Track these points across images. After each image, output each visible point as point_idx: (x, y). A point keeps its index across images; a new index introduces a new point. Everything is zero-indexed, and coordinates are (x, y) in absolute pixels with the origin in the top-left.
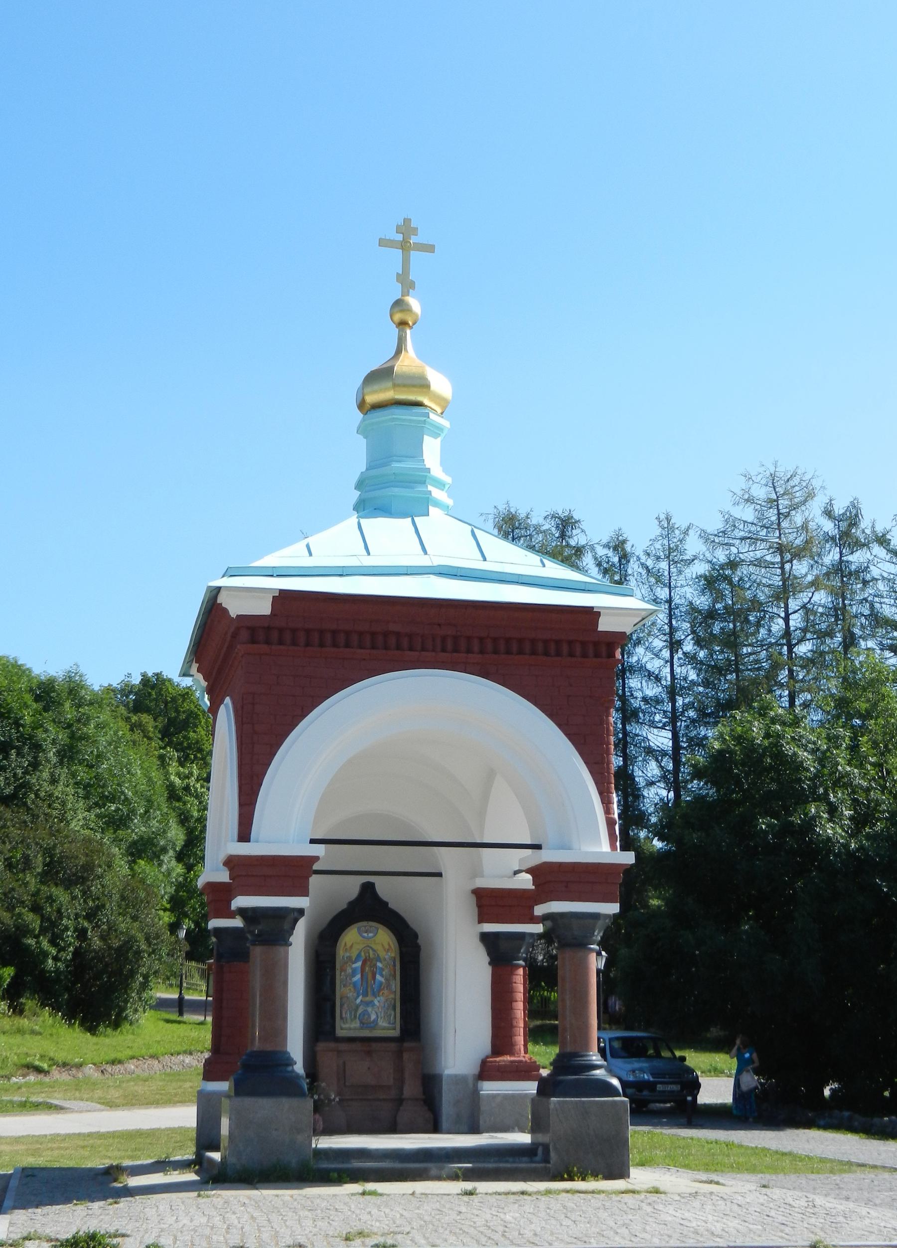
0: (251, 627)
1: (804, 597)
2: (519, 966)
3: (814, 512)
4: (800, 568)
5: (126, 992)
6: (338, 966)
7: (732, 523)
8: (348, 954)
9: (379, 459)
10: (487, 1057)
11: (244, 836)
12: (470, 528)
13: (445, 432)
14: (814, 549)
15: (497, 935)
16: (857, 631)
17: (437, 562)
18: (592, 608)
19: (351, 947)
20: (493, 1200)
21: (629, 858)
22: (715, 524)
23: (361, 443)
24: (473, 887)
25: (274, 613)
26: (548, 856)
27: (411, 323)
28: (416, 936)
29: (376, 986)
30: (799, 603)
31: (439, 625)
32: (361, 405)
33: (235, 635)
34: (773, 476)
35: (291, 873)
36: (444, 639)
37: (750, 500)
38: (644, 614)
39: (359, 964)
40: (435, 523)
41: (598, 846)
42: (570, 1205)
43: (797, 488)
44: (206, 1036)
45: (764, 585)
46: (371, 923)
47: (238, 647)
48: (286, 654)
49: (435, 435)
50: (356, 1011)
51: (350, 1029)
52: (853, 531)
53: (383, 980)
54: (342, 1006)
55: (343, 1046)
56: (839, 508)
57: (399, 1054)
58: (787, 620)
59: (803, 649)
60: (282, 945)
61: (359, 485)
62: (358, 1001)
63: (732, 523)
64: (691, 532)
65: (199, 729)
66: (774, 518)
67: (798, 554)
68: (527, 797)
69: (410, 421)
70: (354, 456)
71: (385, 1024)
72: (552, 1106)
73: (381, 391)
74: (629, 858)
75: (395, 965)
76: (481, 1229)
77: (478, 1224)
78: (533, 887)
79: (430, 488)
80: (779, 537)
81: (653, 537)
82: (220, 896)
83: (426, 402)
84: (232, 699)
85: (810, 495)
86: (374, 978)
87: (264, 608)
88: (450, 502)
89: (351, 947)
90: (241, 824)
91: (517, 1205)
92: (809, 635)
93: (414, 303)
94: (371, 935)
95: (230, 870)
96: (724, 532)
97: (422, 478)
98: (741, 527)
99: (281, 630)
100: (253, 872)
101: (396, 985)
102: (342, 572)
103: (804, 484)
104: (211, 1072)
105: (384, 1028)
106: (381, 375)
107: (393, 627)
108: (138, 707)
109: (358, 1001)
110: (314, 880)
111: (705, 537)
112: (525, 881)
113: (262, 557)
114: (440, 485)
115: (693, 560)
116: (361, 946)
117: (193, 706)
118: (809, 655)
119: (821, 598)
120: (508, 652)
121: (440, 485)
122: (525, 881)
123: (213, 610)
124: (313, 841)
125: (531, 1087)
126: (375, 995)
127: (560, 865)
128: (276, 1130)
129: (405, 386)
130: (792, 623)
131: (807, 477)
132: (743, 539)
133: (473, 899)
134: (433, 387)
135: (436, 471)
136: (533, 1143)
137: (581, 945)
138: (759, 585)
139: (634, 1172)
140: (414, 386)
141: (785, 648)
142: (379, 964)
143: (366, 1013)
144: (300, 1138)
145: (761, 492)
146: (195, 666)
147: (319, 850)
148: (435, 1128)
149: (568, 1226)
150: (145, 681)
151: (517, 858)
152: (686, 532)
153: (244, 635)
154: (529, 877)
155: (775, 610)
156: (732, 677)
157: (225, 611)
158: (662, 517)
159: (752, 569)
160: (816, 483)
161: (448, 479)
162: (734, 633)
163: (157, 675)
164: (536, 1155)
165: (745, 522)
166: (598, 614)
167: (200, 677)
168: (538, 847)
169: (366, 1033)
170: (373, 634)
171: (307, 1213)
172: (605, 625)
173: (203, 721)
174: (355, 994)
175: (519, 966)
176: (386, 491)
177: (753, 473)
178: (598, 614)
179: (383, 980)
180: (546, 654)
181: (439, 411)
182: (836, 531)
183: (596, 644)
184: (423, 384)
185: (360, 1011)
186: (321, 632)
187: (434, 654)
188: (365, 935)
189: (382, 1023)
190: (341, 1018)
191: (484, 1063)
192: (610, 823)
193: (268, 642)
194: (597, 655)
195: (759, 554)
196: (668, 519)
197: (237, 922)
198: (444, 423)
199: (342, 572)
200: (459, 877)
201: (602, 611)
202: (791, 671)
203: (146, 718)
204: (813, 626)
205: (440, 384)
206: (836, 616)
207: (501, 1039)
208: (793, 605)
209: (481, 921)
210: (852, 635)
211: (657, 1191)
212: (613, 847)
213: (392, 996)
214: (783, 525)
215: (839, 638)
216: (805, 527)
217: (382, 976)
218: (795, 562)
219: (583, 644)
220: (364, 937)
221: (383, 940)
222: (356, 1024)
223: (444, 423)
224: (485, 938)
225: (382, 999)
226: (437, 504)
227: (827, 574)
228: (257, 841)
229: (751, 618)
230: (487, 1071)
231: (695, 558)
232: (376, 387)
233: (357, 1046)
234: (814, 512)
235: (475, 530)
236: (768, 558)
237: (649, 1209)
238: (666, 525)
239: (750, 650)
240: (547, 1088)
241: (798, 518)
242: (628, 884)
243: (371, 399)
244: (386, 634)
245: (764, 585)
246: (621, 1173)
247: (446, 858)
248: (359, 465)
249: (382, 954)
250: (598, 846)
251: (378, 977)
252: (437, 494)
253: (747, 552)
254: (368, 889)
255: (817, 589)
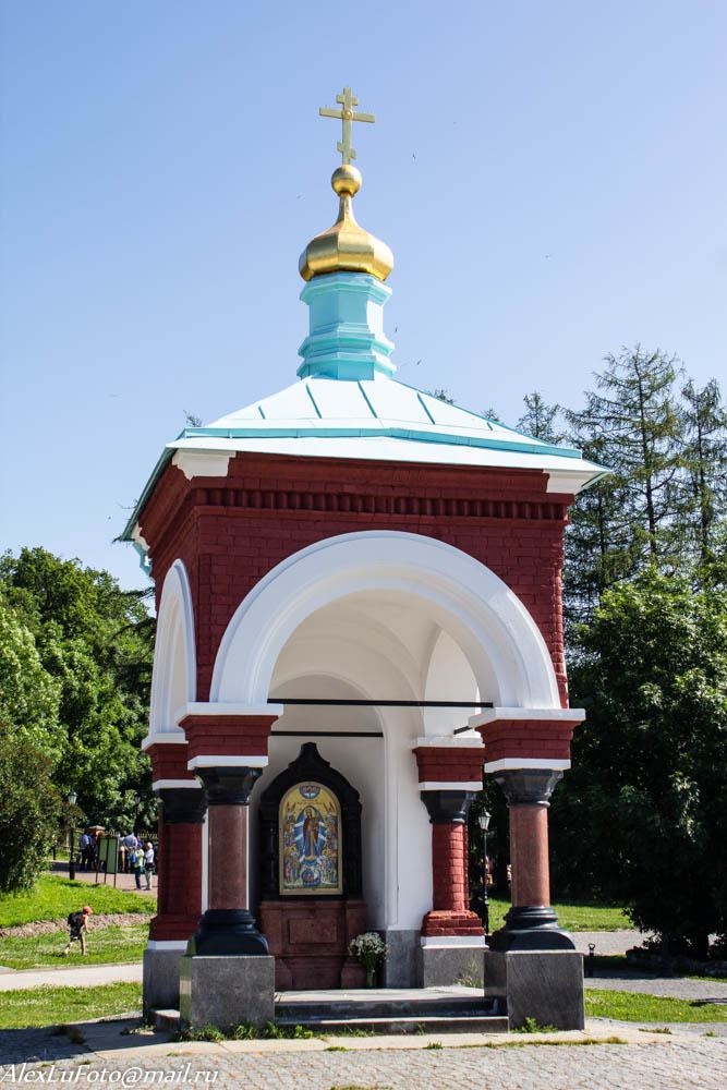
0: (207, 489)
1: (665, 474)
2: (459, 824)
3: (674, 395)
4: (661, 446)
5: (21, 858)
6: (281, 826)
7: (596, 403)
8: (290, 814)
9: (324, 324)
10: (429, 913)
11: (203, 695)
12: (415, 393)
13: (388, 298)
14: (674, 428)
15: (438, 793)
16: (716, 507)
17: (387, 425)
18: (542, 470)
19: (294, 806)
20: (459, 1054)
21: (579, 715)
22: (581, 406)
23: (304, 310)
24: (414, 747)
25: (230, 475)
26: (502, 713)
27: (352, 191)
28: (357, 795)
29: (318, 845)
30: (661, 479)
31: (393, 487)
32: (304, 271)
33: (188, 498)
34: (635, 359)
35: (249, 732)
36: (397, 500)
37: (614, 382)
38: (591, 475)
39: (302, 824)
40: (380, 386)
41: (546, 702)
42: (540, 1057)
43: (658, 370)
44: (152, 895)
45: (629, 463)
46: (313, 783)
47: (195, 508)
48: (229, 521)
49: (379, 301)
50: (299, 869)
51: (293, 888)
52: (711, 411)
53: (325, 839)
54: (285, 865)
55: (288, 905)
56: (698, 389)
57: (342, 911)
58: (649, 495)
59: (665, 523)
60: (241, 804)
61: (303, 351)
62: (301, 860)
63: (596, 403)
64: (558, 413)
65: (79, 603)
66: (636, 399)
67: (658, 434)
68: (485, 658)
69: (324, 289)
70: (298, 325)
71: (327, 883)
72: (508, 960)
73: (326, 257)
74: (579, 715)
75: (336, 825)
76: (463, 1082)
77: (457, 1078)
78: (483, 746)
79: (374, 353)
80: (642, 417)
81: (522, 417)
82: (169, 759)
83: (368, 267)
84: (184, 560)
85: (669, 378)
86: (316, 837)
87: (220, 470)
88: (393, 368)
89: (294, 806)
90: (199, 684)
91: (487, 1058)
92: (670, 510)
93: (353, 171)
94: (312, 794)
95: (186, 731)
96: (589, 413)
97: (365, 344)
98: (605, 407)
99: (237, 492)
100: (203, 732)
101: (338, 844)
102: (297, 434)
103: (665, 366)
104: (157, 931)
105: (327, 887)
106: (327, 242)
107: (349, 489)
108: (19, 581)
109: (301, 860)
110: (271, 740)
111: (572, 417)
112: (473, 739)
113: (215, 420)
114: (383, 350)
115: (560, 439)
116: (303, 807)
117: (71, 581)
118: (671, 529)
119: (682, 474)
120: (460, 513)
121: (383, 350)
122: (473, 739)
123: (167, 471)
124: (270, 701)
125: (479, 943)
126: (317, 854)
127: (513, 722)
128: (238, 988)
129: (349, 253)
130: (654, 499)
131: (667, 360)
132: (607, 418)
133: (414, 756)
134: (377, 255)
135: (380, 338)
136: (486, 997)
137: (532, 801)
138: (623, 462)
139: (588, 1023)
140: (358, 253)
141: (648, 522)
142: (321, 824)
143: (308, 872)
144: (262, 995)
145: (623, 374)
146: (138, 530)
147: (278, 710)
148: (379, 983)
149: (547, 1078)
150: (25, 557)
151: (462, 716)
152: (553, 413)
153: (201, 496)
154: (478, 735)
155: (638, 486)
156: (598, 550)
157: (181, 472)
158: (530, 398)
159: (616, 447)
160: (676, 367)
161: (391, 346)
162: (600, 509)
163: (38, 550)
164: (492, 1008)
165: (609, 402)
166: (548, 476)
167: (142, 541)
168: (490, 705)
169: (309, 892)
170: (328, 496)
171: (283, 1070)
172: (553, 487)
173: (82, 595)
174: (298, 854)
175: (459, 824)
176: (323, 356)
177: (617, 357)
178: (548, 476)
179: (325, 839)
180: (497, 515)
181: (382, 278)
182: (695, 411)
183: (545, 506)
184: (368, 253)
185: (303, 870)
186: (277, 493)
187: (387, 515)
188: (307, 794)
189: (325, 881)
190: (285, 876)
191: (426, 918)
192: (560, 680)
193: (224, 503)
194: (546, 517)
195: (622, 433)
196: (537, 399)
197: (197, 783)
198: (388, 290)
199: (297, 434)
200: (398, 739)
201: (551, 473)
202: (653, 544)
203: (24, 591)
204: (674, 501)
205: (384, 253)
206: (696, 492)
207: (442, 898)
208: (654, 481)
209: (421, 780)
210: (710, 509)
211: (617, 1041)
212: (564, 705)
213: (334, 855)
214: (645, 405)
215: (698, 512)
216: (666, 405)
217: (324, 835)
218: (656, 441)
219: (532, 505)
220: (306, 797)
221: (324, 800)
222: (299, 883)
223: (388, 290)
224: (426, 797)
225: (324, 857)
226: (382, 369)
227: (686, 453)
228: (216, 701)
229: (615, 494)
230: (428, 927)
231: (564, 436)
232: (320, 254)
233: (299, 904)
234: (674, 395)
235: (422, 395)
236: (631, 436)
237: (617, 1059)
238: (534, 405)
239: (614, 524)
240: (498, 942)
241: (659, 399)
242: (576, 740)
243: (314, 265)
244: (340, 496)
245: (629, 463)
246: (578, 1025)
247: (388, 718)
248: (301, 332)
249: (324, 813)
250: (546, 702)
251: (320, 836)
252: (381, 359)
253: (611, 431)
254: (309, 749)
255: (678, 467)
